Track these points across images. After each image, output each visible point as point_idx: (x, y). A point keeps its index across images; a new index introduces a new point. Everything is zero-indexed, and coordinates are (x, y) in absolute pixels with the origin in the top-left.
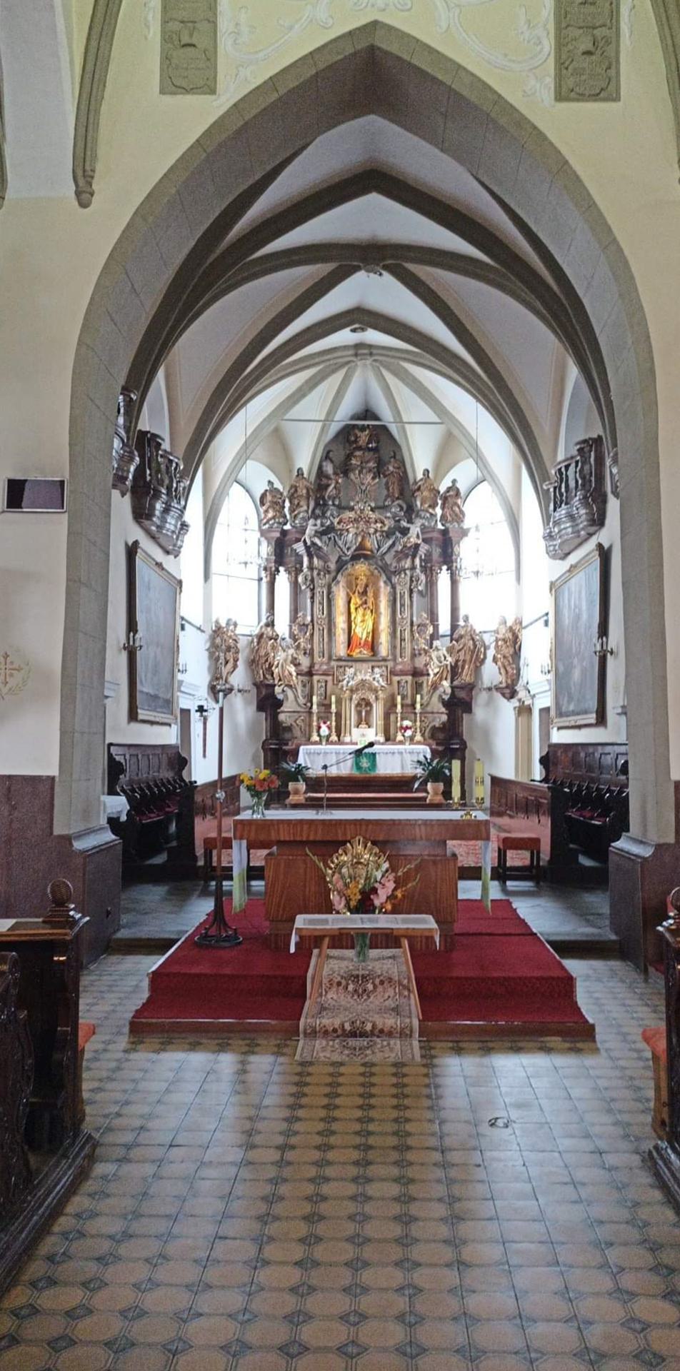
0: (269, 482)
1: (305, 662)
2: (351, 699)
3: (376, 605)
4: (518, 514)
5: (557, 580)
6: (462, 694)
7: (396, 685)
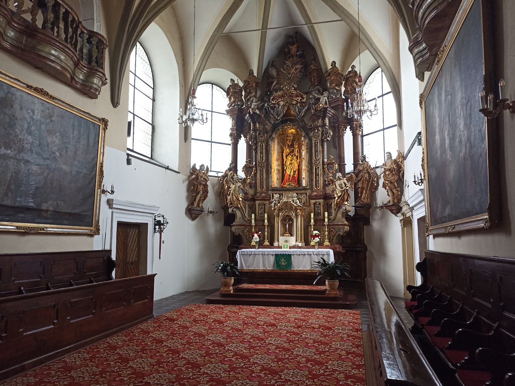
0: (231, 79)
1: (251, 192)
2: (278, 216)
3: (300, 152)
4: (399, 83)
5: (424, 91)
6: (362, 212)
7: (313, 206)
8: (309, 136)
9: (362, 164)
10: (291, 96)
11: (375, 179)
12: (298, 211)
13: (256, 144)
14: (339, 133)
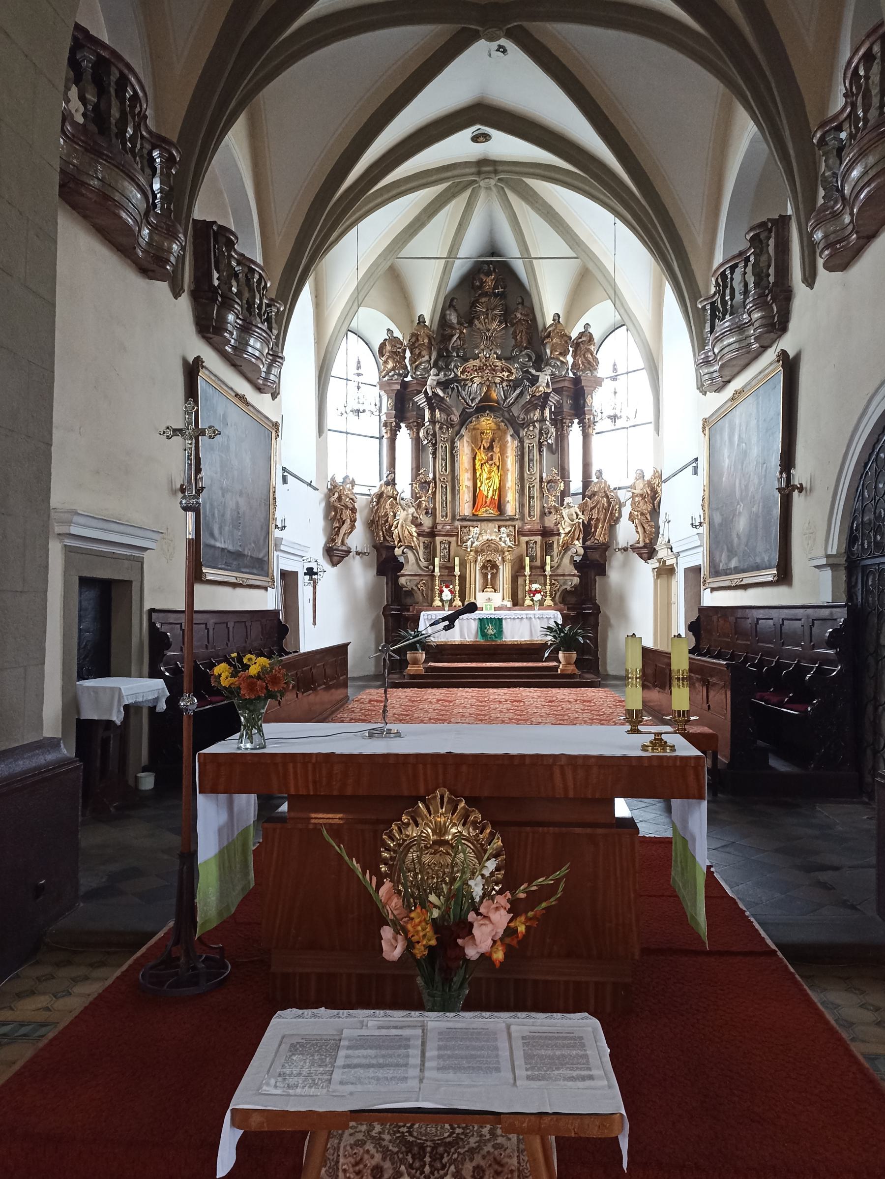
0: (389, 330)
1: (427, 522)
3: (503, 459)
6: (596, 556)
7: (524, 546)
8: (519, 436)
9: (597, 482)
10: (494, 370)
11: (617, 506)
12: (507, 553)
13: (434, 445)
14: (563, 430)
